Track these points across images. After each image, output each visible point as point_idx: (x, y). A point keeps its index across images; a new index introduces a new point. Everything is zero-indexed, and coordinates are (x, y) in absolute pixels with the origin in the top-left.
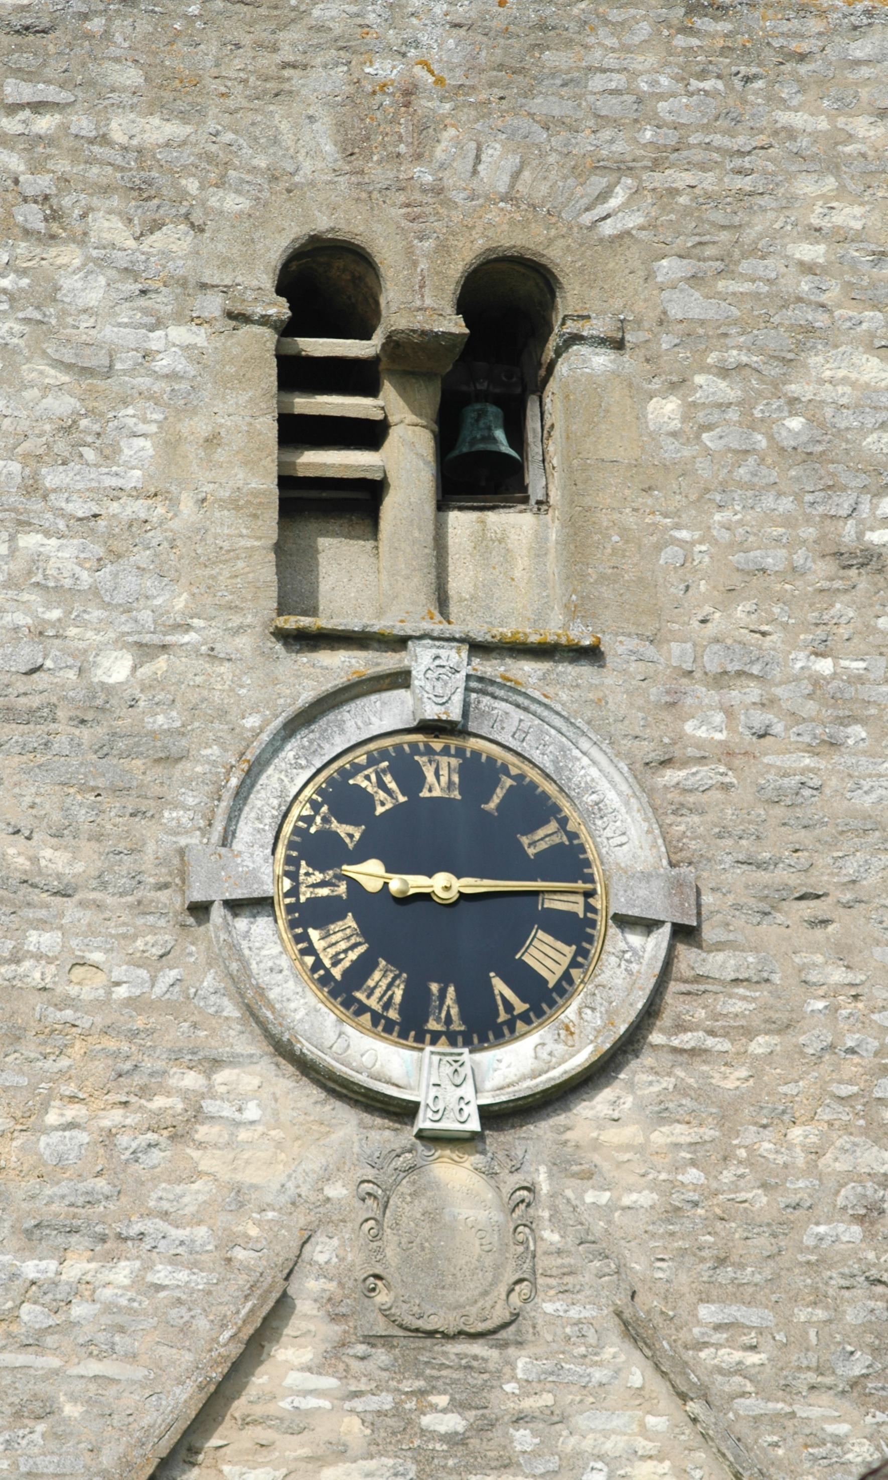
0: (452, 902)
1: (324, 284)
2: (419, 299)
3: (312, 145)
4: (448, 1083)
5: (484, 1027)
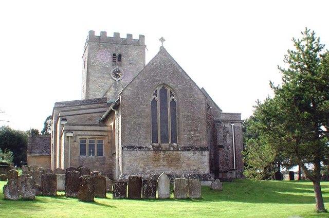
0: (162, 40)
2: (117, 55)
3: (114, 50)
4: (117, 80)
5: (118, 78)
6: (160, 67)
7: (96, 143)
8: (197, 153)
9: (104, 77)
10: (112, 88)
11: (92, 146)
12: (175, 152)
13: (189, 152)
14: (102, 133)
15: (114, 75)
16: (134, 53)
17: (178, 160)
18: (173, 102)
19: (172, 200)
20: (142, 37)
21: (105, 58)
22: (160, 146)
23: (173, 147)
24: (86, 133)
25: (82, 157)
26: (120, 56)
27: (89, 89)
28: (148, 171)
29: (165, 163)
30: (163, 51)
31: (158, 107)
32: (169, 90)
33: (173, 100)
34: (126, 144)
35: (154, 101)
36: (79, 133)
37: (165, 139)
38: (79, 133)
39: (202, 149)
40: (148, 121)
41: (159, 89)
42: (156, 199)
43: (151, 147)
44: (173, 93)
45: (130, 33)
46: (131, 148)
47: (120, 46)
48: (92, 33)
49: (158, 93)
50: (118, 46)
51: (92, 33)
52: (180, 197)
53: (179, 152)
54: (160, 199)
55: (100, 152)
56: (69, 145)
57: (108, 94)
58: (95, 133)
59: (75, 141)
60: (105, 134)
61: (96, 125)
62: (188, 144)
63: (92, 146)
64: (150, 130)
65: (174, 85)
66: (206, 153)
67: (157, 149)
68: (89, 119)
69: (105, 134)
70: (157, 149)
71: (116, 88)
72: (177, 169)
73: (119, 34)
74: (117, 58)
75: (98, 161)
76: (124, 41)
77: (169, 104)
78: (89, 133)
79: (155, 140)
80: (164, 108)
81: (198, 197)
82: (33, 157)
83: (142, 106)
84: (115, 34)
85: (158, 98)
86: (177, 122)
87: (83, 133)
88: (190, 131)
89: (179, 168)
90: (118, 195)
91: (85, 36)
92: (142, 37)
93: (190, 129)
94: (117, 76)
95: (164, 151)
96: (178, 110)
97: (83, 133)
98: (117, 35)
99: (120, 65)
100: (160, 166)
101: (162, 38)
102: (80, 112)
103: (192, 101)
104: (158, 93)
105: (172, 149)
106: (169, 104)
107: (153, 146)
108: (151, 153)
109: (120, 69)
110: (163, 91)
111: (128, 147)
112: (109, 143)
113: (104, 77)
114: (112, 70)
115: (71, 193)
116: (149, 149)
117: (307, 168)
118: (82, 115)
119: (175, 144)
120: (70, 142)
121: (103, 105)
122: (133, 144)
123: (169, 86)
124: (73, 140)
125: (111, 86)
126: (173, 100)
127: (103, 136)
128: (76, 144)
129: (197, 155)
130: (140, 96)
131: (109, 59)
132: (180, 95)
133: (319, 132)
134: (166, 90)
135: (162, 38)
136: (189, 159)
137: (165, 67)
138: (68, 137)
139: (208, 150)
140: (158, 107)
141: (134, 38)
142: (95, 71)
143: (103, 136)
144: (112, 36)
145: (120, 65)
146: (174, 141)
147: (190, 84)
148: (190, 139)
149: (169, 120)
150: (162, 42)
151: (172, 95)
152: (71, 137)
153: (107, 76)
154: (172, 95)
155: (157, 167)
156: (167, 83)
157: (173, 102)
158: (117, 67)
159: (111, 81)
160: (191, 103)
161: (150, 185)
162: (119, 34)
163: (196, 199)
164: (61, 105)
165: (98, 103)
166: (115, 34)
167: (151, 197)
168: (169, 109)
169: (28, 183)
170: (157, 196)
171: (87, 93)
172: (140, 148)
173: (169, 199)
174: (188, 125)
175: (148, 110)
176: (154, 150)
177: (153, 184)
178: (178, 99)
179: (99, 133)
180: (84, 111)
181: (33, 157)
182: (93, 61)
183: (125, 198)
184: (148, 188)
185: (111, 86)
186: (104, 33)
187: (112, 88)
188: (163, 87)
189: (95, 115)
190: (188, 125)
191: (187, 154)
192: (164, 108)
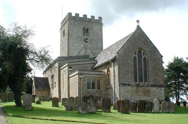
0: (138, 21)
1: (84, 29)
2: (86, 29)
6: (138, 37)
7: (96, 82)
8: (158, 88)
10: (83, 49)
11: (93, 84)
12: (147, 88)
13: (154, 88)
14: (100, 76)
15: (84, 41)
16: (96, 28)
17: (149, 92)
19: (161, 113)
20: (100, 18)
22: (139, 84)
24: (91, 76)
25: (88, 90)
26: (87, 30)
27: (70, 50)
28: (133, 98)
29: (142, 94)
30: (139, 28)
31: (137, 61)
32: (142, 51)
33: (145, 57)
34: (121, 83)
35: (135, 58)
36: (87, 75)
37: (141, 80)
38: (87, 75)
39: (161, 86)
40: (132, 69)
41: (137, 51)
42: (152, 113)
43: (134, 84)
44: (145, 53)
45: (77, 13)
46: (124, 85)
47: (87, 23)
48: (70, 14)
49: (137, 53)
50: (86, 23)
51: (70, 14)
52: (164, 112)
53: (149, 88)
54: (154, 113)
55: (99, 88)
56: (81, 83)
57: (81, 53)
58: (96, 76)
59: (84, 81)
62: (153, 83)
63: (93, 84)
64: (133, 74)
66: (163, 88)
67: (138, 86)
68: (85, 67)
70: (138, 86)
71: (85, 49)
72: (148, 97)
73: (86, 15)
74: (86, 31)
75: (98, 92)
77: (142, 59)
78: (92, 76)
80: (140, 62)
81: (173, 112)
82: (38, 90)
84: (84, 15)
85: (137, 56)
86: (147, 70)
87: (89, 76)
88: (154, 76)
89: (149, 97)
90: (132, 111)
91: (65, 14)
92: (100, 18)
94: (86, 42)
96: (148, 63)
97: (89, 76)
98: (85, 16)
99: (88, 35)
100: (139, 95)
101: (138, 20)
102: (79, 63)
103: (155, 58)
104: (137, 53)
105: (145, 86)
106: (142, 59)
107: (135, 84)
108: (135, 88)
109: (88, 37)
110: (140, 52)
111: (122, 84)
114: (83, 38)
115: (105, 110)
116: (134, 86)
118: (81, 65)
119: (146, 83)
120: (81, 81)
121: (87, 60)
122: (125, 83)
123: (143, 49)
124: (83, 80)
125: (83, 48)
127: (100, 77)
128: (85, 82)
129: (158, 89)
131: (81, 32)
132: (149, 55)
134: (141, 52)
135: (138, 20)
136: (154, 92)
138: (80, 78)
139: (164, 87)
140: (137, 61)
141: (88, 17)
142: (73, 38)
143: (100, 77)
144: (82, 16)
145: (88, 35)
146: (146, 81)
147: (154, 48)
148: (154, 80)
149: (143, 69)
150: (138, 23)
151: (144, 54)
153: (80, 41)
154: (144, 54)
155: (138, 96)
158: (86, 36)
159: (83, 45)
160: (155, 59)
161: (149, 105)
162: (86, 15)
163: (172, 112)
164: (62, 59)
165: (84, 58)
166: (84, 15)
167: (149, 112)
168: (143, 63)
170: (153, 111)
171: (68, 52)
172: (129, 85)
173: (159, 113)
174: (153, 72)
175: (132, 63)
176: (136, 86)
177: (151, 105)
179: (98, 76)
180: (82, 63)
181: (38, 90)
182: (71, 32)
183: (136, 112)
185: (83, 48)
186: (77, 15)
187: (83, 49)
188: (139, 50)
190: (153, 72)
191: (154, 89)
192: (140, 62)
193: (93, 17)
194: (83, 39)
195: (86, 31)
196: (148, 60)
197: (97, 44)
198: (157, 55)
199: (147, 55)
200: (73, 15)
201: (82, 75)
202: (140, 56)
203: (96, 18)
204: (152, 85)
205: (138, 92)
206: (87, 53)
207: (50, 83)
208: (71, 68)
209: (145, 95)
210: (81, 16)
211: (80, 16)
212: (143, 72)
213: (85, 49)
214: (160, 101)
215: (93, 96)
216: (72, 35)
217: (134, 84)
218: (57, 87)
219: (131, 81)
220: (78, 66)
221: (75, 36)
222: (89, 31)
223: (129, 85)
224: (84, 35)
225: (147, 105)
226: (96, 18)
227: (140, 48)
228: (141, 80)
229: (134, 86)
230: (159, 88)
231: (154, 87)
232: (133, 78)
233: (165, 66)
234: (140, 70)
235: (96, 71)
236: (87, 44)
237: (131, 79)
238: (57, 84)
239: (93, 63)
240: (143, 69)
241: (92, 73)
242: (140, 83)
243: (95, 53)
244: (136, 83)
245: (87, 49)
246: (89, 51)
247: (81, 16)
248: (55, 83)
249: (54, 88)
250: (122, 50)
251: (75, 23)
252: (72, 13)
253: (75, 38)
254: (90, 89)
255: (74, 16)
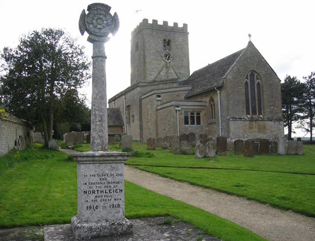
0: (250, 36)
1: (165, 40)
2: (167, 41)
6: (250, 57)
8: (276, 122)
9: (157, 59)
10: (164, 69)
11: (192, 118)
12: (262, 122)
18: (258, 84)
20: (185, 25)
21: (155, 44)
23: (261, 118)
24: (189, 107)
26: (169, 41)
28: (246, 136)
31: (249, 88)
32: (256, 75)
33: (258, 82)
35: (246, 83)
36: (184, 107)
37: (254, 112)
38: (184, 107)
40: (243, 98)
41: (249, 74)
43: (246, 118)
44: (259, 77)
45: (166, 20)
48: (145, 21)
49: (249, 77)
50: (167, 33)
51: (145, 21)
57: (161, 73)
60: (202, 108)
61: (182, 101)
63: (192, 118)
65: (260, 71)
69: (202, 108)
70: (251, 120)
74: (167, 43)
76: (172, 28)
77: (256, 85)
78: (191, 107)
79: (248, 113)
80: (253, 89)
83: (240, 87)
85: (248, 81)
86: (262, 99)
87: (186, 107)
92: (185, 25)
93: (271, 104)
95: (256, 121)
96: (263, 91)
97: (186, 107)
98: (165, 23)
102: (170, 90)
104: (249, 77)
105: (260, 119)
106: (256, 85)
110: (252, 75)
112: (205, 115)
113: (157, 59)
116: (246, 120)
117: (230, 134)
119: (261, 116)
121: (175, 85)
122: (235, 116)
123: (256, 72)
126: (247, 81)
130: (238, 80)
131: (161, 44)
132: (263, 79)
133: (48, 102)
134: (254, 75)
137: (254, 57)
140: (249, 88)
144: (162, 24)
146: (260, 113)
148: (271, 112)
149: (257, 98)
152: (179, 110)
154: (258, 79)
156: (255, 69)
157: (258, 84)
159: (163, 62)
160: (270, 85)
161: (273, 145)
169: (210, 146)
175: (243, 90)
178: (262, 81)
182: (148, 45)
184: (272, 147)
186: (155, 22)
187: (164, 69)
189: (181, 92)
191: (272, 123)
192: (253, 89)
193: (176, 24)
194: (163, 55)
195: (167, 43)
196: (263, 86)
197: (183, 60)
198: (274, 80)
199: (261, 79)
200: (150, 22)
201: (178, 107)
202: (252, 82)
203: (180, 25)
204: (268, 118)
205: (251, 128)
206: (170, 73)
207: (124, 116)
208: (159, 96)
209: (259, 132)
210: (160, 23)
211: (159, 24)
212: (257, 102)
213: (167, 68)
214: (185, 143)
215: (193, 134)
216: (149, 50)
217: (246, 118)
218: (137, 122)
219: (242, 113)
220: (169, 94)
221: (154, 51)
222: (172, 44)
223: (240, 118)
224: (165, 49)
225: (270, 146)
226: (180, 25)
227: (253, 71)
228: (254, 112)
229: (246, 120)
230: (277, 123)
231: (271, 120)
232: (245, 109)
233: (191, 73)
234: (253, 98)
235: (195, 101)
236: (169, 61)
237: (243, 112)
238: (137, 117)
239: (187, 89)
240: (257, 98)
241: (185, 103)
242: (254, 116)
243: (180, 73)
244: (248, 116)
245: (169, 68)
246: (172, 71)
247: (160, 23)
248: (133, 116)
249: (132, 123)
250: (230, 73)
251: (153, 32)
252: (183, 32)
253: (153, 53)
254: (188, 124)
255: (162, 24)
